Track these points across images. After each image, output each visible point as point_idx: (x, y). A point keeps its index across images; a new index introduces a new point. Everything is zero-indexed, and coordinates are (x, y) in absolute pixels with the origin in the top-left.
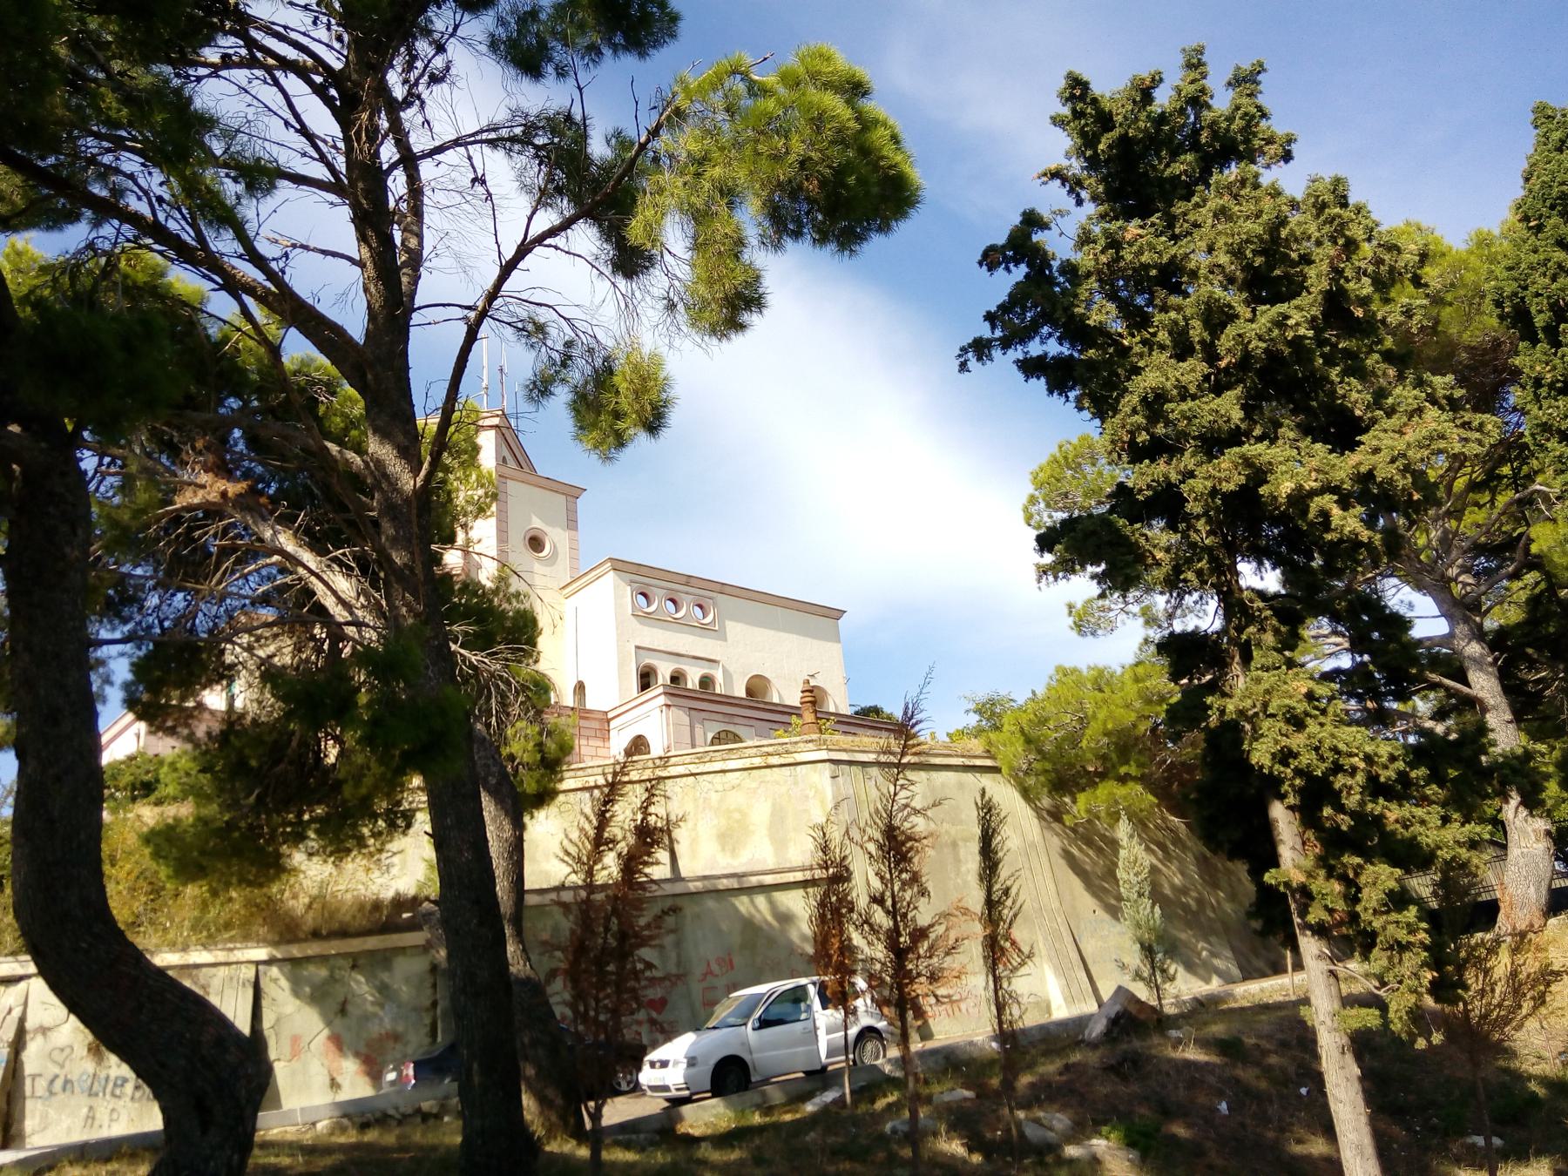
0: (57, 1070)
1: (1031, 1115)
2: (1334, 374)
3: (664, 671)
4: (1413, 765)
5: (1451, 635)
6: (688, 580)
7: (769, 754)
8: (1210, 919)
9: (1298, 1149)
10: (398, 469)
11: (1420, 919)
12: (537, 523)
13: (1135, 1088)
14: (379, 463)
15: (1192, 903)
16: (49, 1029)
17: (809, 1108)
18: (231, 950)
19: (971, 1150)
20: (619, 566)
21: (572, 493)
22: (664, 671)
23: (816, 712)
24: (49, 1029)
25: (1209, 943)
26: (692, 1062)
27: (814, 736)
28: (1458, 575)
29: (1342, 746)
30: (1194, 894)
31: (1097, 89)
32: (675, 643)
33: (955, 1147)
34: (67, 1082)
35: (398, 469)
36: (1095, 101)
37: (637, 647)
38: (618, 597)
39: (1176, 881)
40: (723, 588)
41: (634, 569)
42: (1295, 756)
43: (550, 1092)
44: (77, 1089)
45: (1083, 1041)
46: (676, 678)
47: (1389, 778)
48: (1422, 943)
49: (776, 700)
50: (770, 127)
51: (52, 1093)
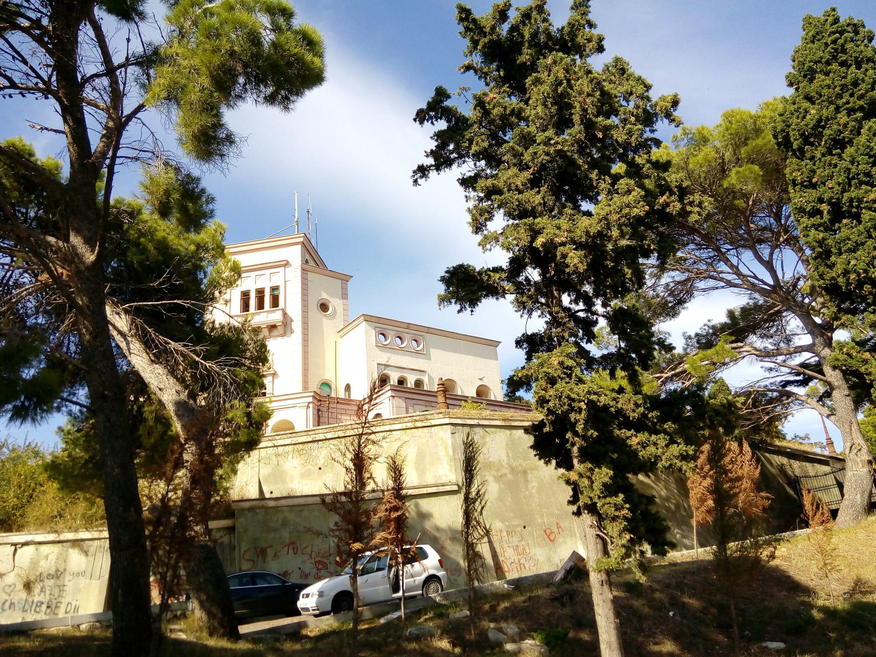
0: (7, 597)
1: (498, 626)
2: (594, 175)
3: (394, 378)
4: (650, 410)
5: (813, 345)
6: (408, 326)
7: (416, 421)
8: (683, 516)
9: (656, 648)
10: (84, 250)
11: (625, 502)
12: (324, 296)
13: (567, 611)
14: (74, 247)
15: (673, 507)
16: (4, 574)
17: (382, 621)
18: (101, 531)
19: (454, 645)
20: (368, 319)
21: (345, 279)
22: (394, 378)
23: (445, 396)
24: (4, 574)
25: (682, 530)
26: (321, 594)
27: (443, 410)
28: (821, 308)
29: (573, 396)
30: (674, 501)
31: (477, 14)
32: (403, 363)
33: (444, 644)
34: (12, 604)
35: (84, 250)
36: (474, 21)
37: (379, 364)
38: (367, 335)
39: (663, 493)
40: (429, 330)
41: (377, 320)
42: (548, 402)
43: (214, 610)
44: (17, 608)
45: (552, 583)
46: (401, 382)
47: (634, 418)
48: (624, 517)
49: (459, 393)
50: (213, 34)
51: (3, 610)
